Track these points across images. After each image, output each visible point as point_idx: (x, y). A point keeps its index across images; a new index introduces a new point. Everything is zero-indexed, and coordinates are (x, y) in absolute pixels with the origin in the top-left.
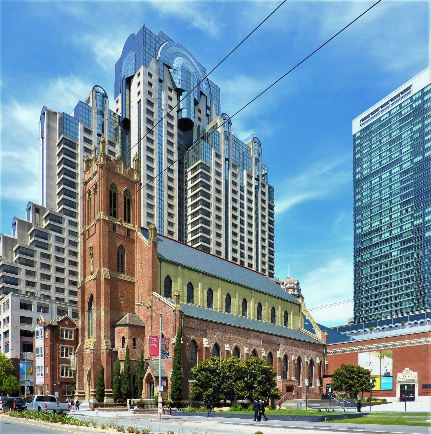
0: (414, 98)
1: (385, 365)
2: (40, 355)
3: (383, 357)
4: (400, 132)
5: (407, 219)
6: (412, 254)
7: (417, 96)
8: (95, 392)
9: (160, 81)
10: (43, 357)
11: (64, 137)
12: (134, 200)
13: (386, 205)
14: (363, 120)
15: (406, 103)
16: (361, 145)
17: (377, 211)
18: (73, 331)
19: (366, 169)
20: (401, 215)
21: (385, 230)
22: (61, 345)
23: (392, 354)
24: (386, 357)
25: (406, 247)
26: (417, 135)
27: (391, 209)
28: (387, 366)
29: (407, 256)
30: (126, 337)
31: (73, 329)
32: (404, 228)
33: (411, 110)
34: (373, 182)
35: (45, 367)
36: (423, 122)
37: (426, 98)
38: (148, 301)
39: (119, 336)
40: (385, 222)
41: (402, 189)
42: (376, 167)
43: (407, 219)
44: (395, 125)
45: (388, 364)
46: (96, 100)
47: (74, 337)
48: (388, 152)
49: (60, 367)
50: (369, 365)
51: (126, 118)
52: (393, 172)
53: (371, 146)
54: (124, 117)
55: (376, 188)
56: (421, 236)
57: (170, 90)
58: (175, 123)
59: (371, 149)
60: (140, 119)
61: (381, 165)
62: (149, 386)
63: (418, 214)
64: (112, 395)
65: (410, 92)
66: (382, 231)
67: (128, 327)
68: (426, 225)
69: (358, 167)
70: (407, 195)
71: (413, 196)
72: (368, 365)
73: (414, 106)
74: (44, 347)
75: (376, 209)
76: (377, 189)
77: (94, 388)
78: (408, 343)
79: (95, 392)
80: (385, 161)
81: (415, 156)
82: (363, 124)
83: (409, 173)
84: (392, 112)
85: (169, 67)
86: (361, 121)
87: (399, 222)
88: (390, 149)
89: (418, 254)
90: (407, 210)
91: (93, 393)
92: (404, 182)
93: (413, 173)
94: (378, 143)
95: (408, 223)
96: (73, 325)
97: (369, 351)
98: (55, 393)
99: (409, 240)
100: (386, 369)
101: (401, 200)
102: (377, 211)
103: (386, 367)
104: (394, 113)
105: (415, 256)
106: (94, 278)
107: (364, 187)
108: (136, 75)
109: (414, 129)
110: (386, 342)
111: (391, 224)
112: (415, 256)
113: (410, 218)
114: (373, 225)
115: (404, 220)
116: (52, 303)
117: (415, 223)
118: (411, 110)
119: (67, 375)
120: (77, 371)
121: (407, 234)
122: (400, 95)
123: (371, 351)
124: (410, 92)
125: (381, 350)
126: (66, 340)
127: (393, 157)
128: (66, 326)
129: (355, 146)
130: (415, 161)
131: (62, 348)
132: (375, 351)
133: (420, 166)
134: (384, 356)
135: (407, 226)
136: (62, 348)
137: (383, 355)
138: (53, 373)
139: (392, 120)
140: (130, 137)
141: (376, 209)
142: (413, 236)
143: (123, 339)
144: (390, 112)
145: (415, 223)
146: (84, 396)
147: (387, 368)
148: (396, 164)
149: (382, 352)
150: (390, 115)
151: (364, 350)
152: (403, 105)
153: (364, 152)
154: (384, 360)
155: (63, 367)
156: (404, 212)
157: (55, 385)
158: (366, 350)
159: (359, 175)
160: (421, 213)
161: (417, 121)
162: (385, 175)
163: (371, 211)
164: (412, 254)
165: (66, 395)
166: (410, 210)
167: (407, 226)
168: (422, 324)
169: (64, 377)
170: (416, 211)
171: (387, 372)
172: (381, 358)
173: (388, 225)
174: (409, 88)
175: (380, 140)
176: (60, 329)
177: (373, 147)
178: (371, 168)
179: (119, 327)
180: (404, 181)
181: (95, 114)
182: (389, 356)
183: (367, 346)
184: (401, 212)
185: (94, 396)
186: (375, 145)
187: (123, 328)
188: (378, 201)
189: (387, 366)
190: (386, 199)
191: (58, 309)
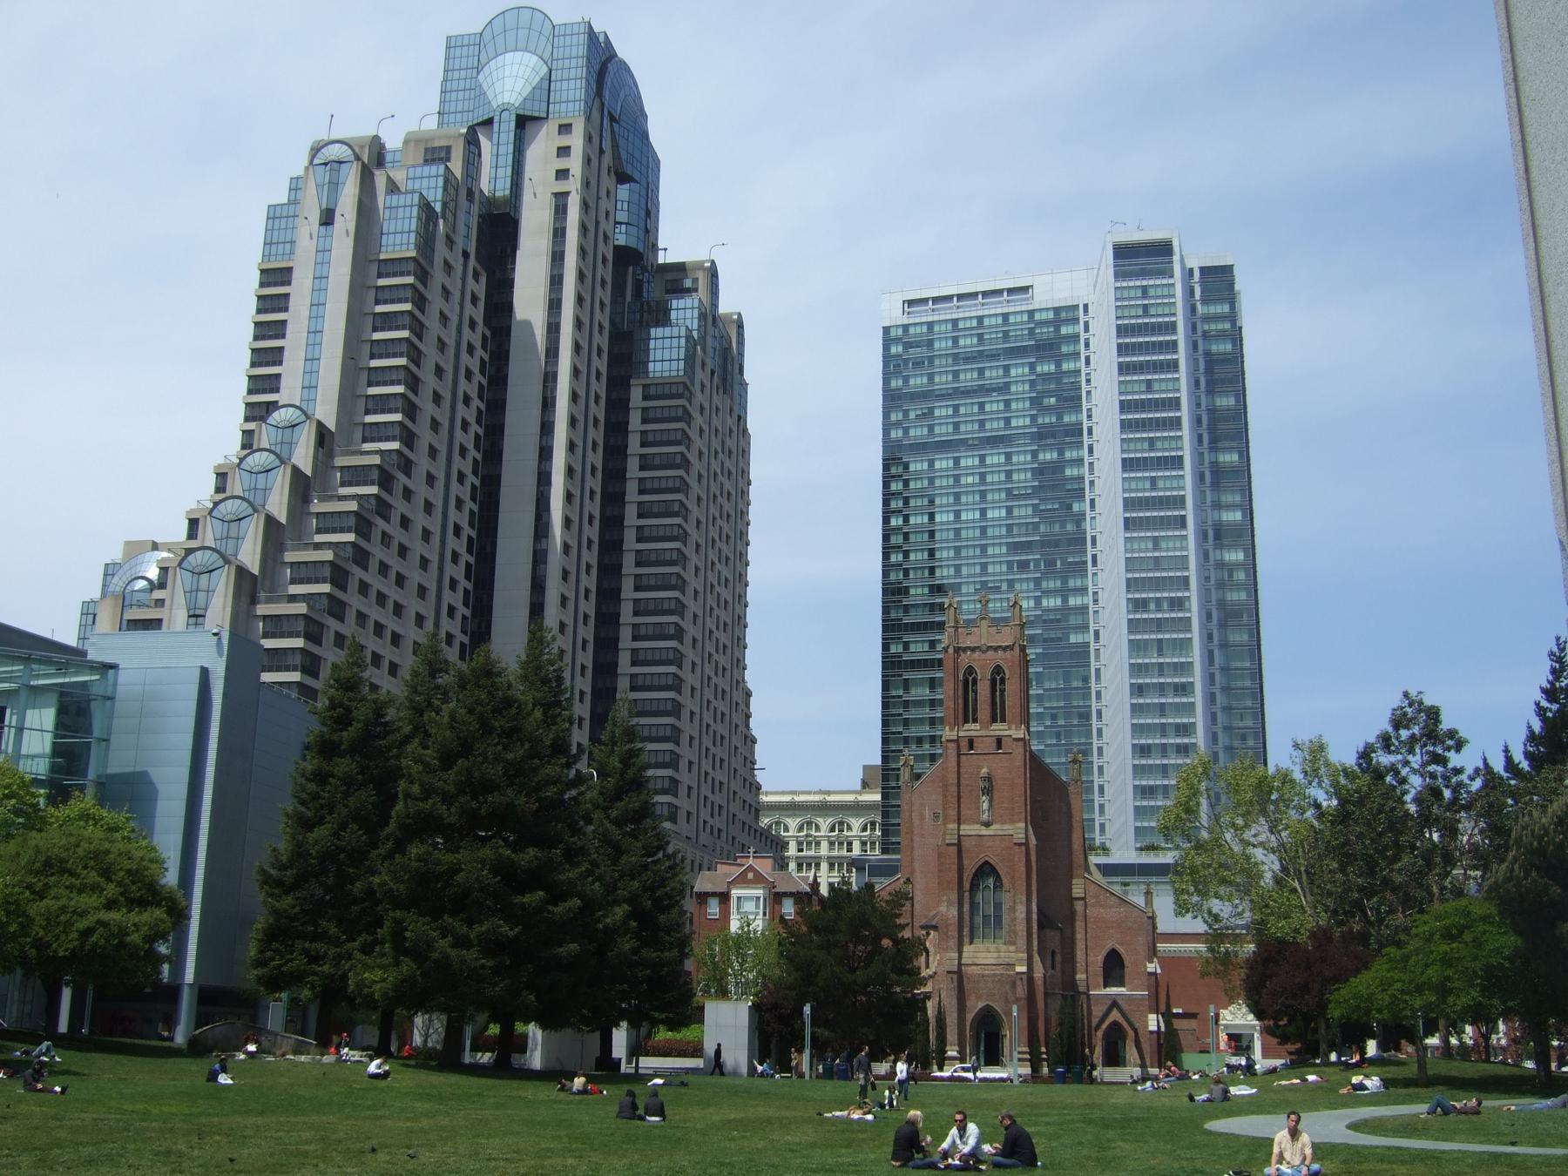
65: (1027, 299)
81: (1044, 448)
170: (1046, 575)
173: (978, 587)
185: (1030, 1060)
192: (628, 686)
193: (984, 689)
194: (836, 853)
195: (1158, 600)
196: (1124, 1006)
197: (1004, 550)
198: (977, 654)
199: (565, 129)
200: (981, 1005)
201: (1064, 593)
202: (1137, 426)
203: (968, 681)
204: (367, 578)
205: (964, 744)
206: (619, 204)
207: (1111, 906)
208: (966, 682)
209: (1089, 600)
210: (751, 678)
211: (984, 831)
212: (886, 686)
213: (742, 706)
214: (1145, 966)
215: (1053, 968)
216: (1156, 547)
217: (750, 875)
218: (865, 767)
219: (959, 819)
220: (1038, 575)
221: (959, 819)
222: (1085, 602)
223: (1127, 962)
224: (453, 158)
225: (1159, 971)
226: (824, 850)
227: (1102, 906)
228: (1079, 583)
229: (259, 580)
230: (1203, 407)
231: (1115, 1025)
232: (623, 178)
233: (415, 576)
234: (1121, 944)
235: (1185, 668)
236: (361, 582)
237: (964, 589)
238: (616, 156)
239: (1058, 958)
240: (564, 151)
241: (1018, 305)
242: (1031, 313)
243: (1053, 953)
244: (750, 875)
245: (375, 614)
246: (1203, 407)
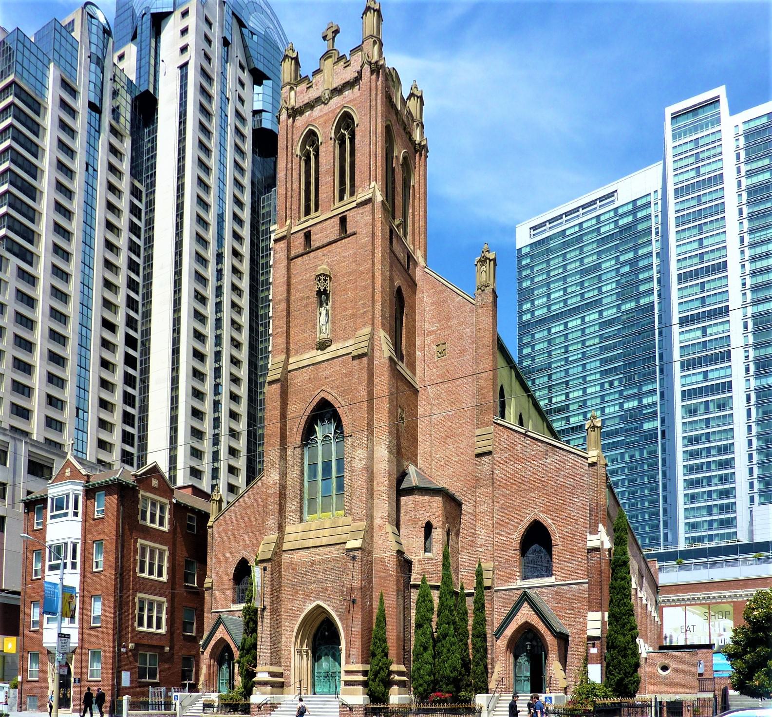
0: (620, 211)
1: (717, 632)
2: (69, 565)
3: (713, 617)
4: (598, 259)
5: (612, 397)
6: (622, 454)
7: (625, 209)
8: (365, 673)
9: (226, 43)
10: (78, 570)
11: (17, 80)
12: (413, 186)
13: (575, 371)
14: (534, 228)
15: (607, 216)
16: (532, 268)
17: (561, 378)
18: (168, 507)
19: (541, 307)
20: (601, 391)
21: (574, 410)
22: (140, 541)
23: (732, 612)
24: (720, 617)
25: (612, 443)
26: (627, 269)
27: (584, 377)
28: (722, 632)
29: (614, 457)
30: (435, 523)
31: (166, 501)
32: (607, 411)
33: (615, 228)
34: (553, 331)
35: (87, 598)
36: (635, 249)
37: (639, 215)
38: (476, 439)
39: (415, 520)
40: (575, 398)
41: (603, 349)
42: (557, 306)
43: (612, 397)
44: (590, 247)
45: (724, 630)
46: (90, 31)
47: (169, 523)
48: (579, 288)
49: (136, 600)
50: (686, 630)
51: (147, 91)
52: (587, 319)
53: (548, 273)
54: (143, 89)
55: (558, 341)
56: (636, 428)
57: (242, 67)
58: (248, 131)
59: (549, 276)
60: (186, 102)
61: (566, 305)
62: (512, 659)
63: (630, 392)
64: (404, 681)
65: (613, 201)
66: (569, 412)
67: (440, 499)
68: (644, 412)
69: (527, 303)
70: (611, 360)
71: (622, 363)
72: (684, 630)
73: (621, 223)
74: (84, 545)
75: (558, 375)
76: (560, 343)
77: (365, 661)
78: (719, 597)
79: (365, 673)
80: (574, 300)
81: (625, 301)
82: (534, 235)
83: (614, 326)
84: (585, 225)
85: (241, 24)
86: (530, 228)
87: (598, 400)
88: (582, 283)
89: (632, 457)
90: (611, 383)
91: (360, 678)
92: (607, 339)
93: (621, 326)
94: (561, 270)
95: (615, 405)
96: (169, 491)
97: (685, 605)
98: (123, 672)
99: (616, 433)
100: (720, 638)
101: (601, 366)
102: (561, 378)
103: (720, 635)
104: (588, 228)
105: (627, 458)
106: (354, 353)
107: (537, 336)
108: (177, 14)
109: (622, 259)
110: (718, 590)
111: (585, 401)
112: (627, 458)
113: (617, 396)
114: (554, 400)
115: (607, 399)
116: (17, 442)
117: (626, 406)
118: (615, 228)
119: (150, 625)
120: (267, 613)
121: (612, 422)
122: (598, 202)
123: (688, 605)
124: (613, 201)
125: (709, 604)
126: (152, 528)
127: (586, 296)
128: (153, 490)
129: (521, 269)
130: (623, 308)
131: (143, 549)
132: (696, 604)
133: (632, 317)
134: (717, 615)
135: (612, 409)
136: (143, 549)
137: (713, 614)
138: (120, 615)
139: (585, 238)
140: (155, 131)
141: (558, 375)
142: (623, 426)
143: (428, 528)
144: (581, 224)
145: (626, 406)
146: (282, 685)
147: (722, 638)
148: (576, 315)
149: (711, 609)
150: (581, 229)
151: (676, 602)
152: (602, 218)
153: (536, 280)
154: (717, 623)
155: (142, 602)
156: (607, 386)
157: (123, 650)
158: (693, 602)
159: (529, 316)
160: (636, 391)
161: (626, 247)
162: (575, 323)
163: (550, 376)
164: (622, 454)
165: (147, 680)
166: (616, 383)
167: (612, 409)
168: (713, 565)
169: (144, 628)
170: (627, 387)
171: (723, 644)
172: (709, 618)
173: (581, 404)
174: (612, 194)
175: (565, 266)
176: (140, 496)
177: (552, 274)
178: (549, 307)
179: (417, 497)
180: (606, 337)
181: (85, 59)
182: (725, 615)
183: (680, 596)
184: (602, 385)
185: (365, 684)
186: (556, 272)
187: (427, 498)
188: (563, 363)
189: (722, 632)
190: (575, 361)
191: (31, 459)
197: (598, 376)
199: (185, 14)
200: (309, 607)
202: (691, 276)
205: (298, 243)
206: (256, 96)
207: (533, 458)
211: (321, 356)
214: (585, 540)
216: (704, 334)
217: (68, 472)
219: (288, 349)
221: (288, 349)
223: (556, 538)
224: (75, 30)
225: (608, 545)
227: (519, 461)
228: (650, 387)
231: (527, 630)
232: (258, 77)
234: (547, 512)
237: (571, 408)
238: (248, 57)
240: (184, 31)
241: (604, 210)
242: (616, 210)
244: (68, 472)
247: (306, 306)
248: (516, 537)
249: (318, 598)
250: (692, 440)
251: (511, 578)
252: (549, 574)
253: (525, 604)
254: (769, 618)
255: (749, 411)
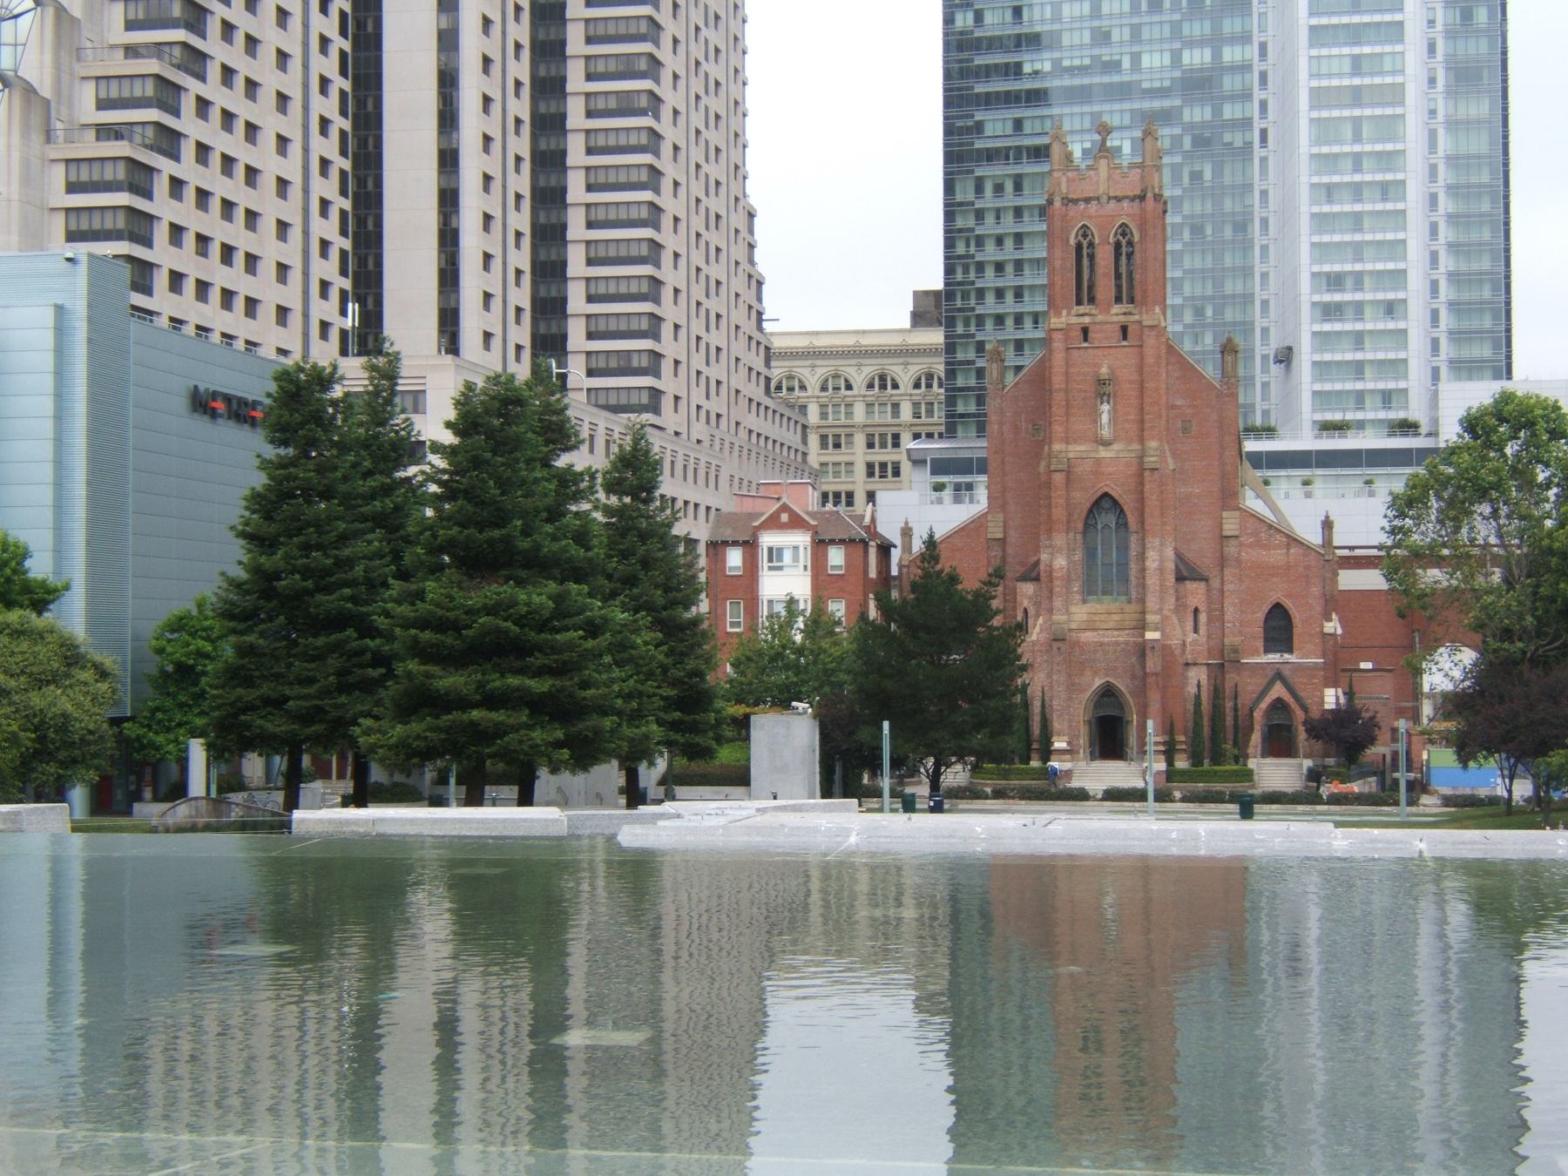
30: (1201, 608)
192: (582, 221)
193: (1104, 256)
194: (877, 419)
195: (1357, 122)
196: (1296, 681)
198: (1093, 208)
200: (1098, 682)
201: (1216, 41)
203: (1083, 253)
204: (206, 91)
205: (1078, 334)
208: (1079, 247)
209: (1252, 52)
210: (757, 192)
212: (949, 188)
213: (744, 233)
215: (1196, 630)
217: (784, 517)
218: (915, 293)
220: (1177, 17)
222: (1248, 56)
225: (1339, 631)
226: (859, 413)
227: (1264, 547)
229: (53, 104)
230: (1440, 117)
233: (271, 81)
234: (1289, 596)
235: (1397, 248)
236: (199, 99)
239: (1203, 618)
243: (1196, 610)
244: (784, 517)
245: (223, 143)
246: (1440, 117)
247: (1084, 399)
248: (1260, 615)
249: (1107, 676)
250: (1326, 162)
251: (1255, 653)
252: (1290, 651)
253: (1278, 682)
254: (1567, 519)
255: (1433, 135)
